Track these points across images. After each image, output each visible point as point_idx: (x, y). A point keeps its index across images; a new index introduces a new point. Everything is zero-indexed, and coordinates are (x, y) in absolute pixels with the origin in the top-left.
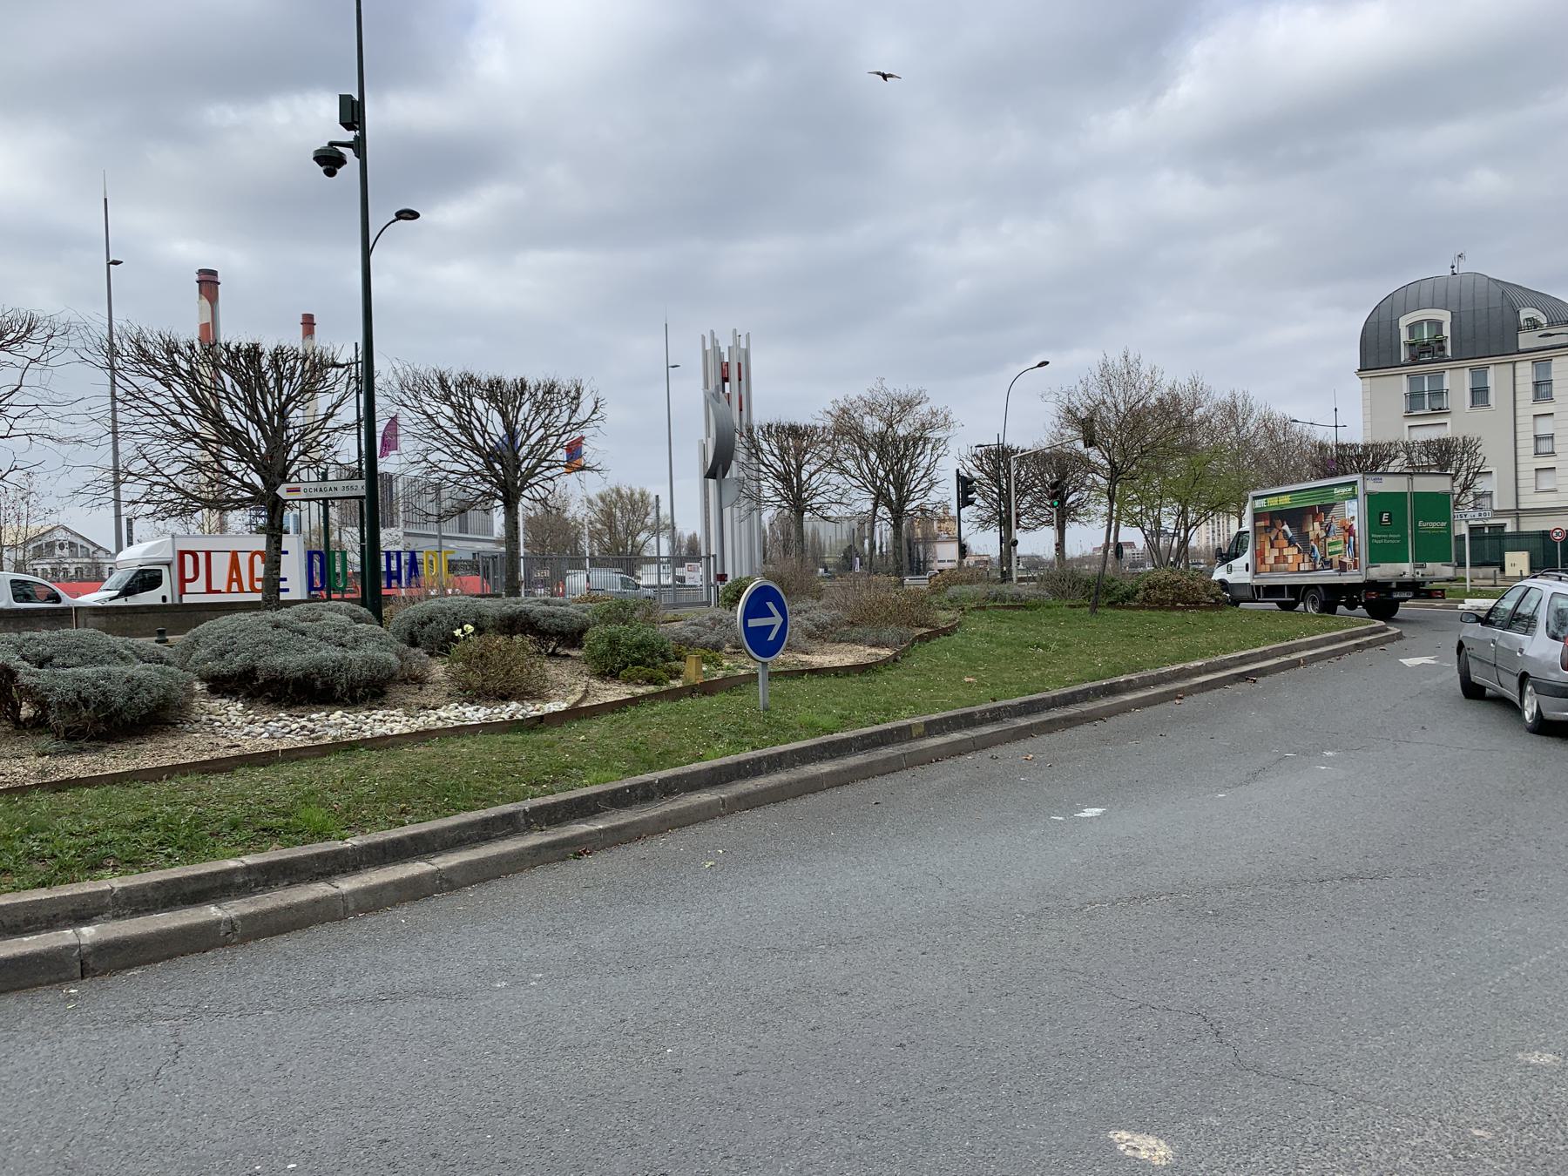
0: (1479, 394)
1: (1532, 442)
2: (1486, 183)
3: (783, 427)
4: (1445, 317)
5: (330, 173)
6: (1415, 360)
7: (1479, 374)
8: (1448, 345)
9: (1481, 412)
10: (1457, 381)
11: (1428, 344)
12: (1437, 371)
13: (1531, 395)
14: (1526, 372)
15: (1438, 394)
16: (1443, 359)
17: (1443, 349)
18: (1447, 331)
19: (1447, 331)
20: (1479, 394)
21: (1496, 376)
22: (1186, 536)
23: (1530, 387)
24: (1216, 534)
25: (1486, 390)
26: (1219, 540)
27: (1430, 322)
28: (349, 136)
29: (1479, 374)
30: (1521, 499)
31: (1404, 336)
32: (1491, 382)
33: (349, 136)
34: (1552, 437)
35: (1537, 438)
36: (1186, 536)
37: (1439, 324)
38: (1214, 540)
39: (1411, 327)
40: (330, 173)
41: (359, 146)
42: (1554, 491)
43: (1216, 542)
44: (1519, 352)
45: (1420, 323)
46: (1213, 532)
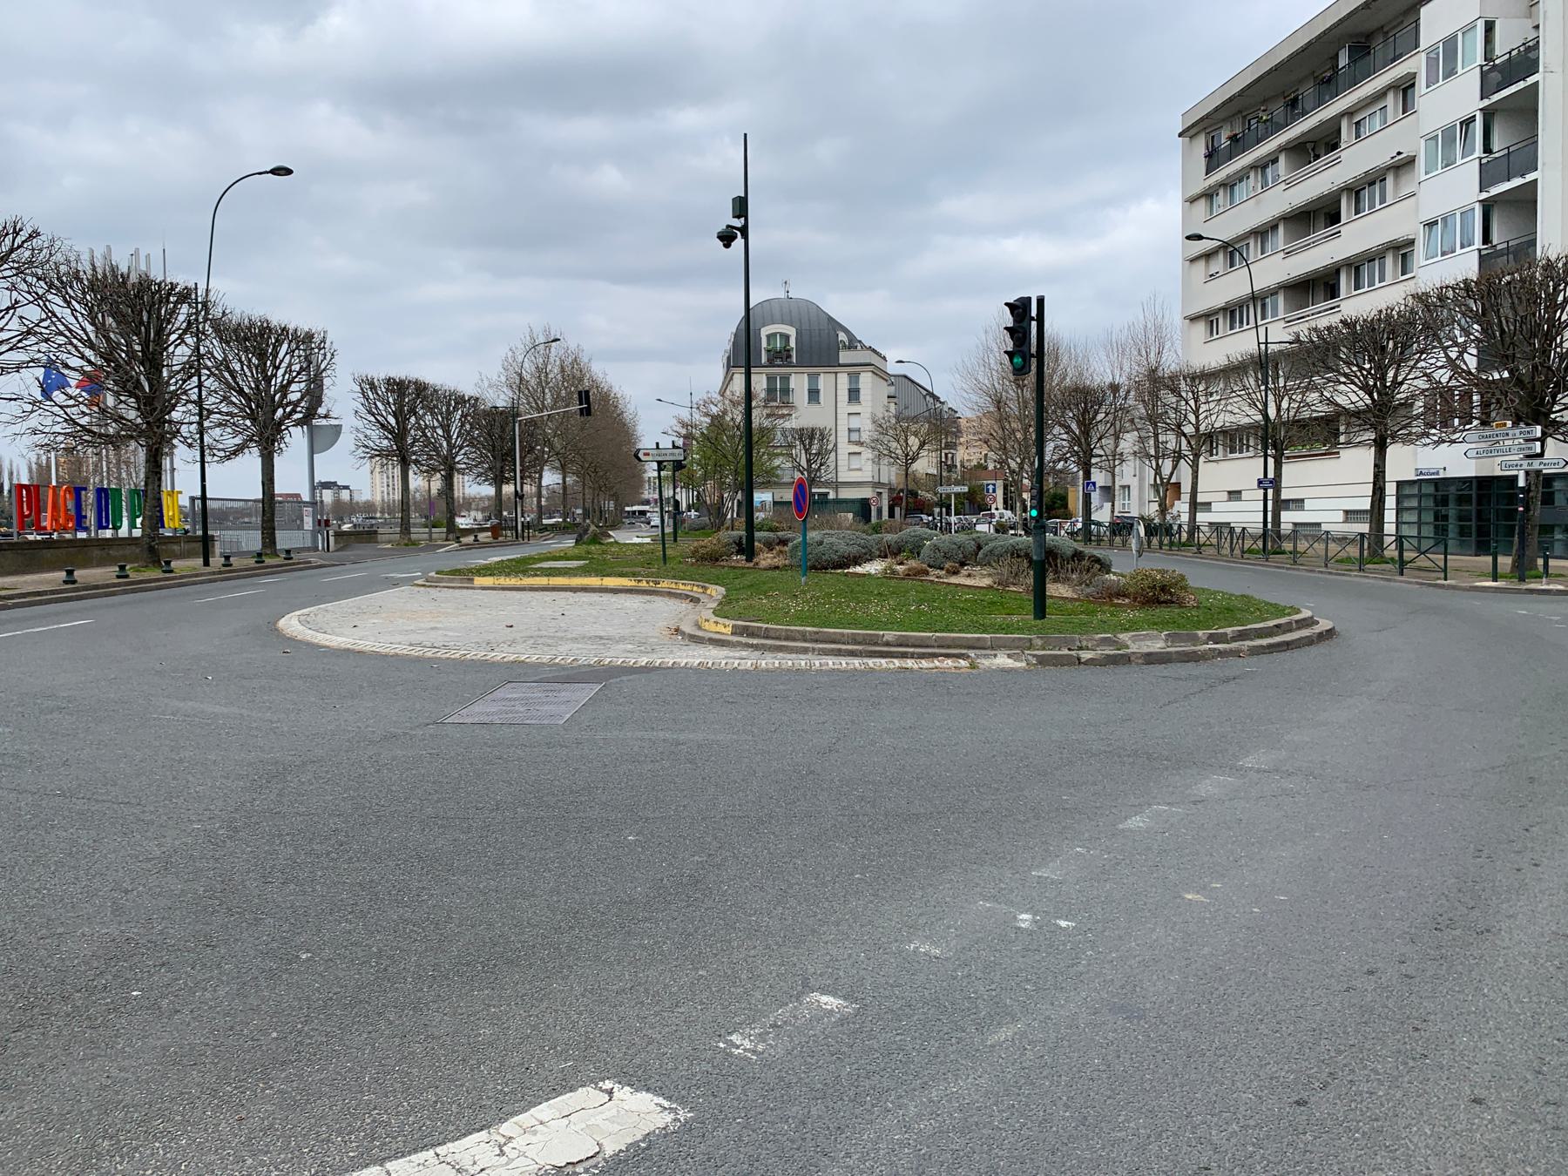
0: (814, 394)
1: (847, 432)
2: (610, 179)
3: (394, 380)
4: (791, 332)
5: (727, 246)
6: (771, 364)
7: (813, 378)
8: (794, 354)
9: (815, 407)
10: (799, 382)
11: (780, 352)
12: (786, 374)
13: (846, 398)
14: (843, 379)
15: (786, 391)
16: (790, 365)
17: (789, 356)
18: (793, 344)
19: (793, 344)
20: (814, 394)
21: (824, 382)
22: (1157, 464)
23: (846, 392)
24: (390, 488)
25: (818, 391)
26: (394, 494)
27: (782, 335)
28: (739, 223)
29: (813, 378)
30: (839, 474)
31: (764, 344)
32: (821, 386)
33: (739, 223)
34: (859, 430)
35: (850, 430)
36: (1157, 464)
37: (786, 337)
38: (388, 494)
39: (769, 337)
40: (727, 246)
41: (744, 231)
42: (860, 470)
43: (391, 496)
44: (840, 365)
45: (774, 335)
46: (388, 486)
